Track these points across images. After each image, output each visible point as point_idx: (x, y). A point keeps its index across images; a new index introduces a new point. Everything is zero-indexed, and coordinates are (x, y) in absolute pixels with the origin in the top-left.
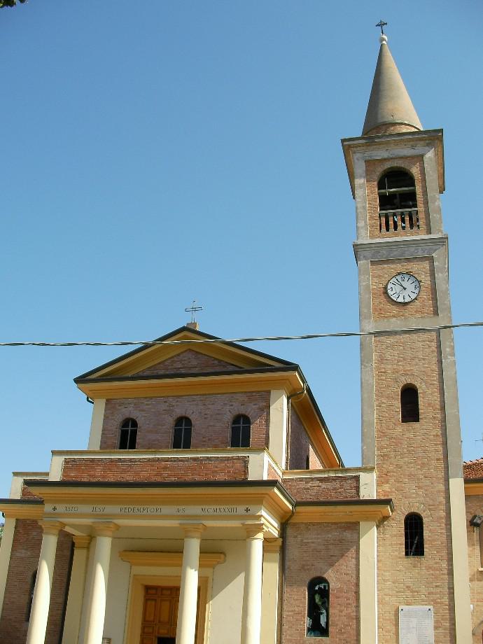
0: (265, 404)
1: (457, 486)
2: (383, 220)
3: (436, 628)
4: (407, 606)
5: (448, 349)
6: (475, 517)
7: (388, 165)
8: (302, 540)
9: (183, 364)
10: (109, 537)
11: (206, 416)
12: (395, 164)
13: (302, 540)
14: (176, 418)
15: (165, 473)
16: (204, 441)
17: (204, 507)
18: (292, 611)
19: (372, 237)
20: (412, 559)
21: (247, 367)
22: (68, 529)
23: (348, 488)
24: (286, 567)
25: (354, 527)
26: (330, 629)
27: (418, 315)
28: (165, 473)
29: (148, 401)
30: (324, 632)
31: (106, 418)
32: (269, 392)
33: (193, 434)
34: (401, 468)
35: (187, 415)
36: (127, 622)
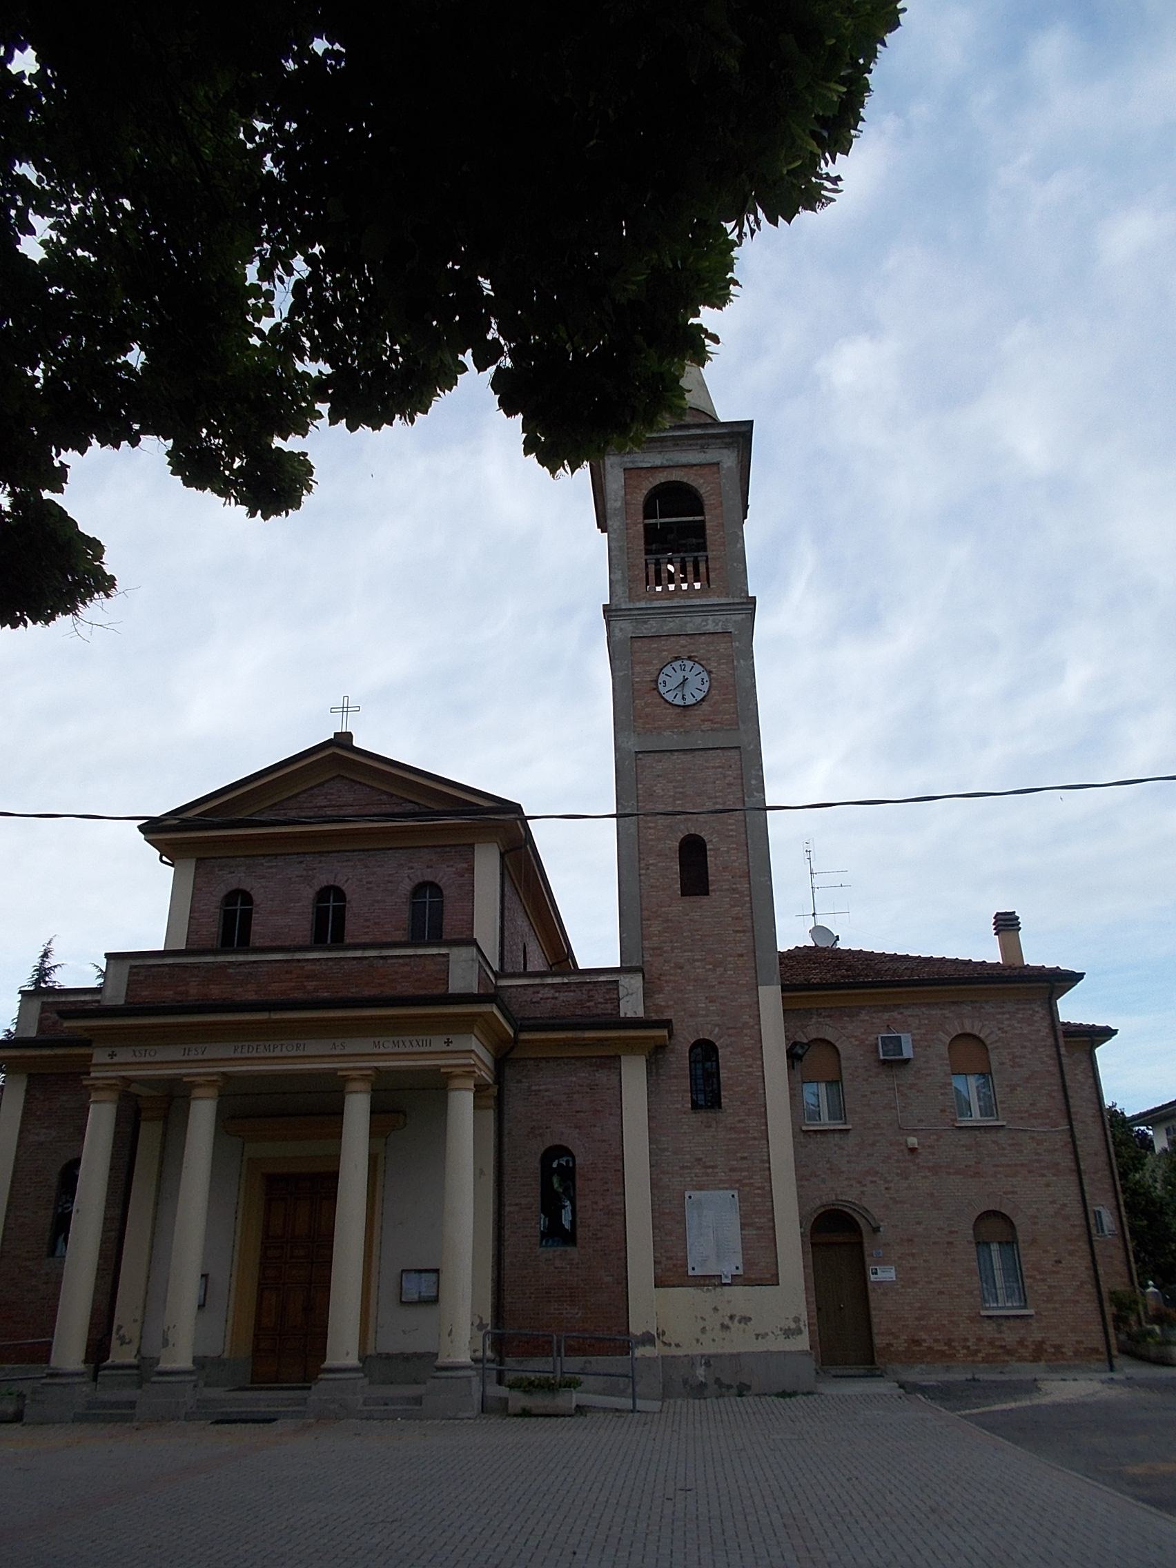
0: (465, 865)
1: (770, 998)
2: (652, 568)
3: (743, 1226)
4: (698, 1192)
5: (753, 782)
6: (795, 1044)
7: (661, 478)
8: (529, 1087)
9: (330, 800)
10: (212, 1098)
11: (369, 886)
12: (676, 476)
13: (529, 1087)
14: (317, 888)
15: (311, 985)
16: (368, 927)
17: (377, 1040)
18: (516, 1205)
19: (631, 599)
20: (703, 1115)
21: (436, 807)
22: (134, 1089)
23: (602, 1000)
24: (506, 1132)
25: (612, 1062)
26: (580, 1232)
27: (706, 726)
28: (311, 985)
29: (269, 861)
30: (569, 1238)
31: (196, 888)
32: (472, 846)
33: (348, 915)
34: (681, 968)
35: (336, 884)
36: (234, 1285)
